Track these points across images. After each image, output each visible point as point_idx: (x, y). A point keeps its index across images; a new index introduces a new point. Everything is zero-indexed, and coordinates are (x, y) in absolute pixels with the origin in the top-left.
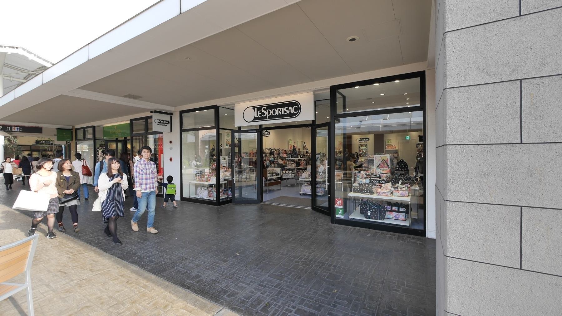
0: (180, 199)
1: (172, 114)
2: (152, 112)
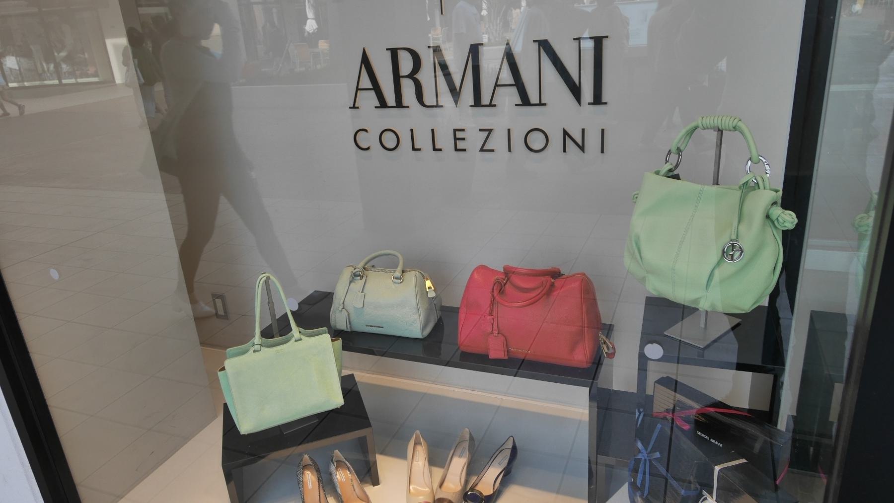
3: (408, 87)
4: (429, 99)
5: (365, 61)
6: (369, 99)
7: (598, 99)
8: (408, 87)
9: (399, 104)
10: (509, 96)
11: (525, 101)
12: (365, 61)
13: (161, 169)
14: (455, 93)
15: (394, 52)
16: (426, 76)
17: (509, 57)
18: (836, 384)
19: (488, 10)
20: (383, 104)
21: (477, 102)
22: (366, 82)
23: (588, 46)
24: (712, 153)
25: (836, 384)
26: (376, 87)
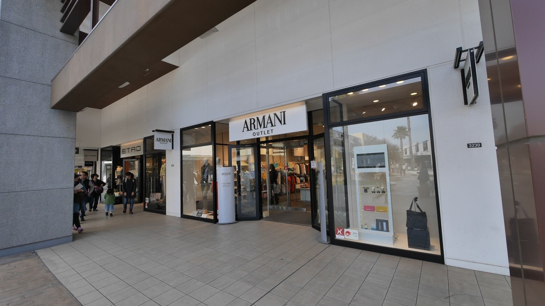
0: (180, 216)
1: (173, 132)
2: (153, 131)
3: (253, 125)
4: (256, 128)
5: (246, 122)
6: (246, 129)
7: (284, 123)
8: (253, 125)
9: (251, 129)
10: (270, 125)
11: (272, 126)
12: (246, 122)
13: (327, 234)
14: (261, 126)
15: (251, 119)
16: (256, 123)
17: (269, 117)
18: (155, 148)
19: (352, 97)
20: (248, 130)
21: (264, 127)
22: (246, 126)
23: (282, 113)
24: (512, 173)
25: (155, 148)
26: (247, 127)
